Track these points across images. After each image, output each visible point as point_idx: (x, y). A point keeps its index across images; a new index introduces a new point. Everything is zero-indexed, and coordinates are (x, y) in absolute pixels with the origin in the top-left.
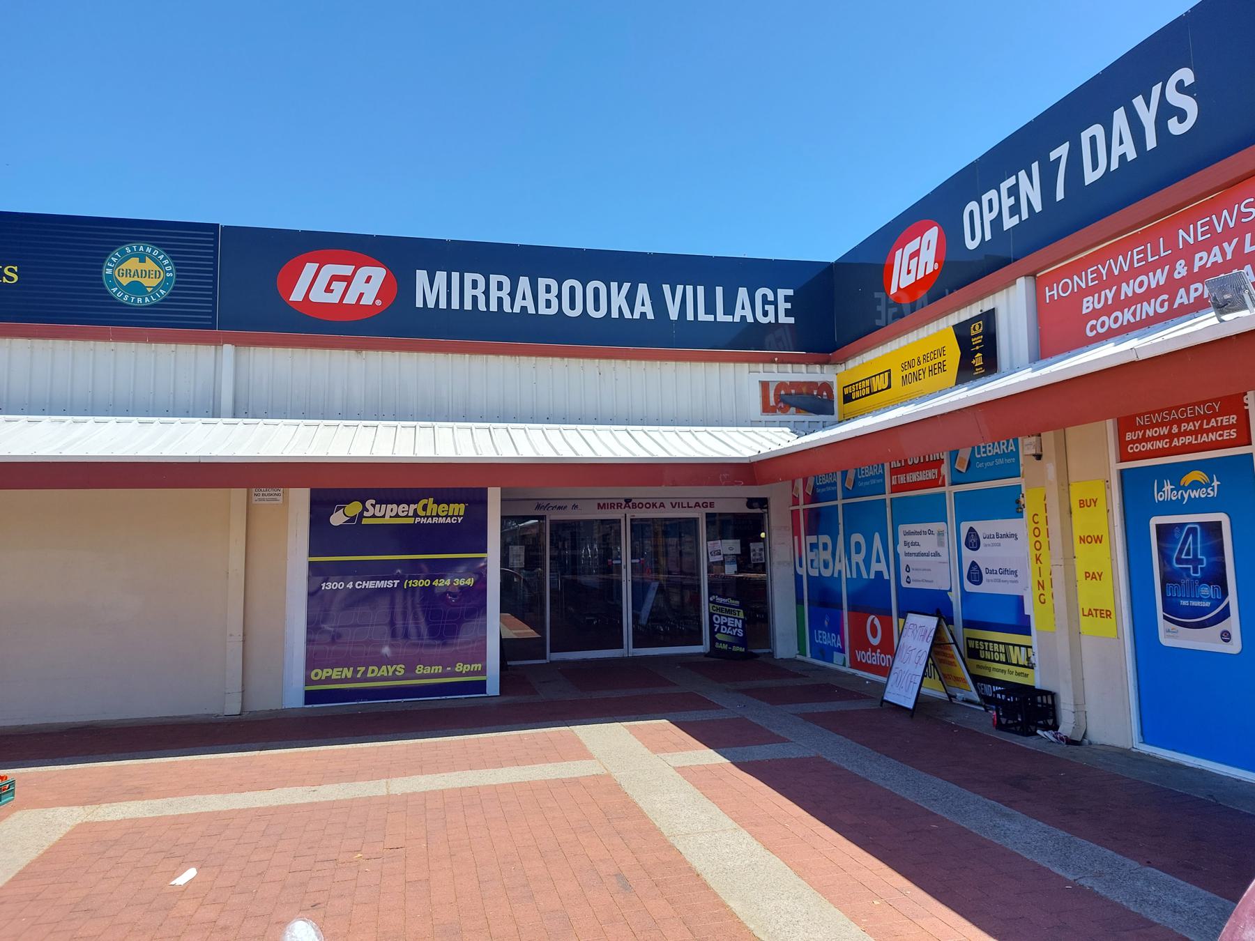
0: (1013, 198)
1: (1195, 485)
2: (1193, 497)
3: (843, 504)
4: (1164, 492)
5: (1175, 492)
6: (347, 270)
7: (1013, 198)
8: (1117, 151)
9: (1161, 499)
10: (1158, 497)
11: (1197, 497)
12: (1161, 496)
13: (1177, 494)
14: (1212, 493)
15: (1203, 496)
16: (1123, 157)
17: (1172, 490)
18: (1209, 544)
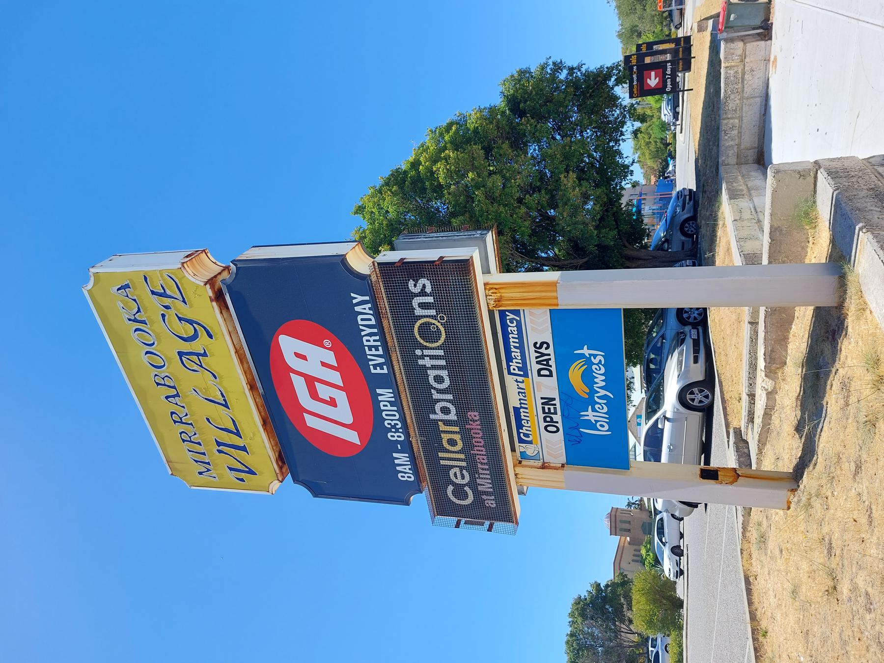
0: (373, 349)
1: (588, 377)
2: (604, 384)
3: (651, 647)
4: (597, 421)
5: (597, 406)
6: (299, 384)
7: (373, 349)
8: (367, 311)
9: (607, 427)
10: (604, 430)
11: (604, 378)
12: (602, 426)
13: (600, 404)
14: (599, 358)
15: (603, 371)
16: (370, 309)
17: (594, 410)
18: (685, 46)
